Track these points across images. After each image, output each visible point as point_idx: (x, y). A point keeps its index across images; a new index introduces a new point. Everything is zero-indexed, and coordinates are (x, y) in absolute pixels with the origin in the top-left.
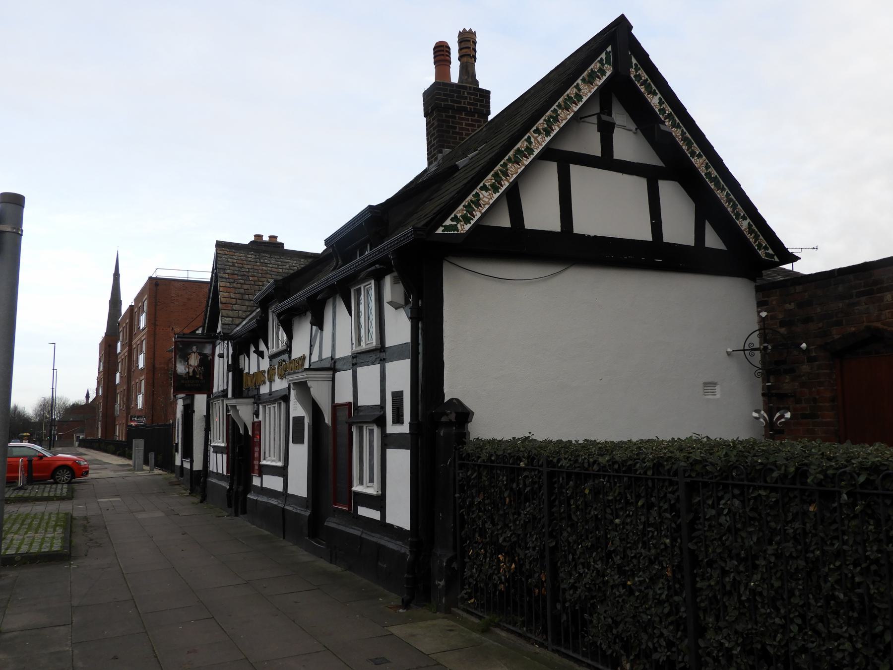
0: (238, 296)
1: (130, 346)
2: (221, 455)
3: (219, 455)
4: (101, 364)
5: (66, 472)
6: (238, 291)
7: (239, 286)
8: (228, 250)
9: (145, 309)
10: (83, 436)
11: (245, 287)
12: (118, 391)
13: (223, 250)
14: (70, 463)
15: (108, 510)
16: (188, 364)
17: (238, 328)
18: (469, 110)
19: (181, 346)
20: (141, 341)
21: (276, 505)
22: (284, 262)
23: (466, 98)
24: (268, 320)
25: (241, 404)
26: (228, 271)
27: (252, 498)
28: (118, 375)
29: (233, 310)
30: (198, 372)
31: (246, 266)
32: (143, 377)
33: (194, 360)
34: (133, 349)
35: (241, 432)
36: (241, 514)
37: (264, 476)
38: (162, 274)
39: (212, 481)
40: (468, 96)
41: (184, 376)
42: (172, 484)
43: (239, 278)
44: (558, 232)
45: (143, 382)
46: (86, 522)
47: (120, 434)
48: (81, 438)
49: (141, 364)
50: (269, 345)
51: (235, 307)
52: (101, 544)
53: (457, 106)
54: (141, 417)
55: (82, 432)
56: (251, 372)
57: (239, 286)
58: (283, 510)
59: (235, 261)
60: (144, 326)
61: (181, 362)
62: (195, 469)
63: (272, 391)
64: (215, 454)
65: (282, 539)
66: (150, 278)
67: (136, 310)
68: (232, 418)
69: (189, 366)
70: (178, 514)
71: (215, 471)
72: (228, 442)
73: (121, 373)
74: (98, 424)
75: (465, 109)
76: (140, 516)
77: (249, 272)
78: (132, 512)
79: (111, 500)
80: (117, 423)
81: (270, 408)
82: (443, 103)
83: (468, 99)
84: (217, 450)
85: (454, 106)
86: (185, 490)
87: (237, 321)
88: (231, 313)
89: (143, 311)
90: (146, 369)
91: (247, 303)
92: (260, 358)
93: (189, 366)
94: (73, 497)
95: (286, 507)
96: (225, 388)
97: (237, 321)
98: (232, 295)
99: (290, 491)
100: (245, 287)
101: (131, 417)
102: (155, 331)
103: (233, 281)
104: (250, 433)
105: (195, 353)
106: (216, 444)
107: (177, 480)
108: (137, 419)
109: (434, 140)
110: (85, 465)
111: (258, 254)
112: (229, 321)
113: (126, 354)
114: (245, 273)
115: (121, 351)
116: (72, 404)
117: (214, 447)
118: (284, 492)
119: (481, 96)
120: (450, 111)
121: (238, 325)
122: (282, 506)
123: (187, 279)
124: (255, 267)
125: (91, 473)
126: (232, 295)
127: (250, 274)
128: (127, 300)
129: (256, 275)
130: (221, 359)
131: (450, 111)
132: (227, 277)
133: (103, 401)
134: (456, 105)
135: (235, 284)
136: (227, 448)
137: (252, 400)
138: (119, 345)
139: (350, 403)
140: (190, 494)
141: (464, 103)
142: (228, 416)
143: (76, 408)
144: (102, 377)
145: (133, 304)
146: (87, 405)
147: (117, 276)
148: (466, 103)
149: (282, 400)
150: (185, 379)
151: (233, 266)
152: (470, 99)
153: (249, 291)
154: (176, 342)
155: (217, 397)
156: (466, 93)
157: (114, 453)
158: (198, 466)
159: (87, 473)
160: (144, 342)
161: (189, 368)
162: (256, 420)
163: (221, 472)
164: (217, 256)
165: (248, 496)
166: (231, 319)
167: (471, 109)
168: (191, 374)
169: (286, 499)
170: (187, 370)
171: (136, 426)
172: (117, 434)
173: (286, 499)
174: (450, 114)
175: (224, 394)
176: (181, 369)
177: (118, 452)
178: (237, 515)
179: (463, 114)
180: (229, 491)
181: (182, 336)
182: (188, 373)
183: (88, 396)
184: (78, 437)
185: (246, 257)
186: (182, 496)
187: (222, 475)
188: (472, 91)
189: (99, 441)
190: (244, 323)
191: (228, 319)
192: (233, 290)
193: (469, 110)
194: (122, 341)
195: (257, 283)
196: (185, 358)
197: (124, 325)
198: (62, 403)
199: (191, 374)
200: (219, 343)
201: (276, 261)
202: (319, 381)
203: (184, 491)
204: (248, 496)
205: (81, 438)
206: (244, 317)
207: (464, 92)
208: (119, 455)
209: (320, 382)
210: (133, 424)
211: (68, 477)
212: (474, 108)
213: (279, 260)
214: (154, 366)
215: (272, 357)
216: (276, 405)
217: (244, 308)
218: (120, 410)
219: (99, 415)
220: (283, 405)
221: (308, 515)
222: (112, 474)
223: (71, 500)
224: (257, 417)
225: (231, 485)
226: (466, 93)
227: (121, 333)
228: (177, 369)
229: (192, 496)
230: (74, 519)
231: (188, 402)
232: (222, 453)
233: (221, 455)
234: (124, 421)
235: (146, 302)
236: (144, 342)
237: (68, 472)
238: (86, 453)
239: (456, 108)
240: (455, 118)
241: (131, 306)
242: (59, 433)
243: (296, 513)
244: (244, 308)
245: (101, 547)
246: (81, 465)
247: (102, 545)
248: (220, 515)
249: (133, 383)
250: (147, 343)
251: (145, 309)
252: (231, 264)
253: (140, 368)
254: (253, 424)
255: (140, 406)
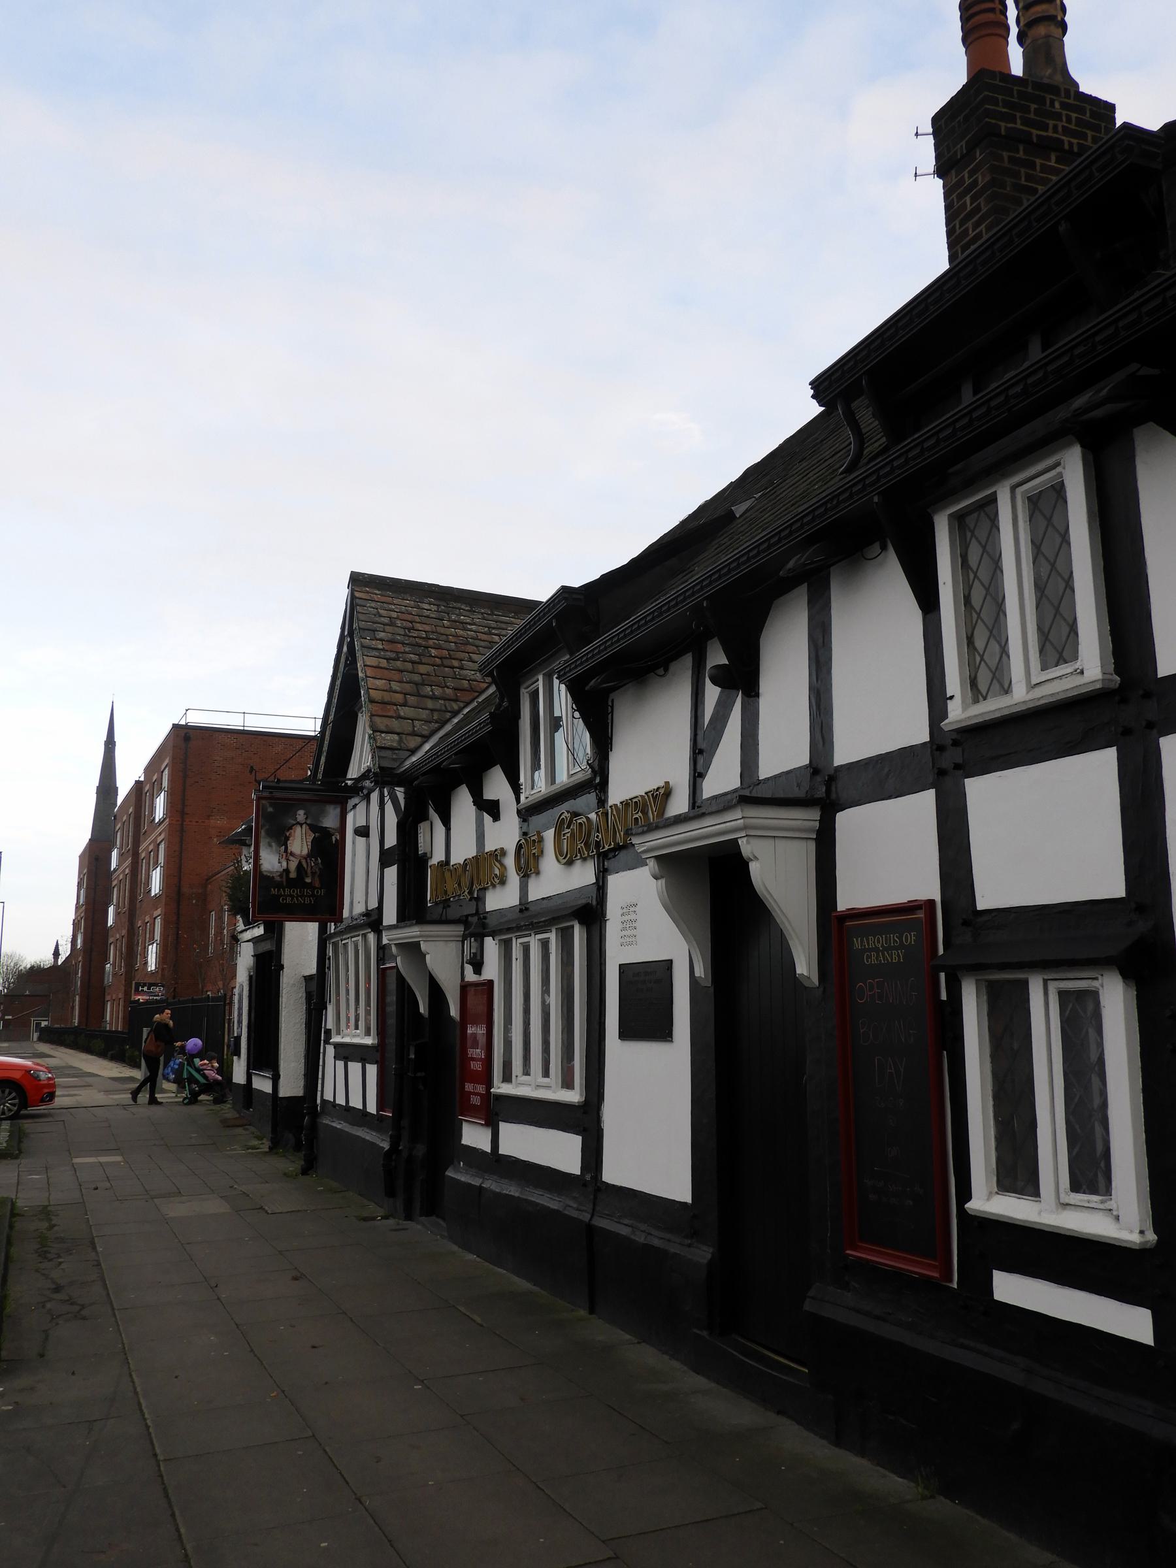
0: (408, 687)
1: (136, 854)
2: (360, 1065)
3: (355, 1067)
4: (82, 892)
5: (10, 1094)
6: (406, 677)
7: (409, 666)
8: (377, 592)
9: (165, 783)
10: (46, 1023)
11: (423, 669)
12: (111, 940)
13: (368, 592)
14: (17, 1075)
15: (96, 1189)
16: (286, 850)
17: (414, 759)
18: (1066, 147)
19: (270, 809)
20: (158, 846)
21: (558, 1211)
22: (502, 622)
23: (1058, 116)
24: (517, 716)
25: (429, 938)
26: (382, 635)
27: (463, 1179)
28: (111, 910)
29: (399, 717)
30: (309, 871)
31: (418, 626)
32: (159, 911)
33: (300, 842)
34: (140, 861)
35: (422, 1010)
36: (421, 1216)
37: (504, 1127)
38: (197, 719)
39: (334, 1125)
40: (1064, 112)
41: (278, 879)
42: (227, 1124)
43: (407, 649)
44: (319, 924)
45: (158, 921)
46: (46, 1225)
47: (113, 1017)
48: (43, 1026)
49: (156, 887)
50: (522, 780)
51: (403, 711)
52: (83, 1307)
53: (1037, 136)
54: (156, 985)
55: (45, 1015)
56: (457, 858)
57: (409, 666)
58: (590, 1229)
59: (394, 615)
60: (161, 815)
61: (270, 845)
62: (283, 1093)
63: (531, 898)
64: (340, 1064)
65: (582, 1313)
66: (175, 726)
67: (147, 788)
68: (401, 980)
69: (288, 854)
70: (261, 1208)
71: (341, 1100)
72: (381, 1033)
73: (117, 907)
74: (74, 1001)
75: (1056, 145)
76: (177, 1209)
77: (428, 638)
78: (152, 1198)
79: (103, 1159)
80: (108, 998)
81: (526, 949)
82: (1003, 124)
83: (1064, 119)
84: (346, 1053)
85: (1031, 133)
86: (260, 1138)
87: (412, 742)
88: (395, 724)
89: (161, 789)
90: (164, 896)
91: (430, 704)
92: (487, 818)
93: (288, 854)
94: (20, 1152)
95: (602, 1223)
96: (373, 904)
97: (412, 742)
98: (395, 686)
99: (610, 1175)
100: (423, 669)
101: (138, 985)
102: (182, 824)
103: (393, 655)
104: (454, 1011)
105: (301, 825)
106: (347, 1040)
107: (238, 1116)
108: (149, 989)
109: (977, 225)
110: (49, 1079)
111: (445, 604)
112: (392, 741)
113: (127, 871)
114: (420, 641)
115: (119, 865)
116: (29, 966)
117: (337, 1046)
118: (588, 1177)
119: (1094, 114)
120: (1021, 148)
121: (413, 752)
122: (586, 1217)
123: (242, 728)
124: (440, 629)
125: (59, 1096)
126: (395, 686)
127: (431, 642)
128: (127, 778)
129: (444, 646)
130: (361, 841)
131: (1021, 148)
132: (380, 647)
133: (83, 957)
134: (1035, 132)
135: (398, 664)
136: (380, 1047)
137: (459, 929)
138: (115, 854)
139: (931, 903)
140: (270, 1148)
141: (1055, 127)
142: (382, 974)
143: (35, 973)
144: (82, 915)
145: (142, 779)
146: (54, 968)
147: (110, 744)
148: (1060, 129)
149: (576, 918)
150: (279, 885)
151: (392, 624)
152: (1069, 120)
153: (433, 678)
154: (259, 799)
155: (353, 928)
156: (1057, 105)
157: (102, 1054)
158: (291, 1085)
159: (52, 1096)
160: (162, 847)
161: (288, 860)
162: (470, 976)
163: (360, 1107)
164: (353, 605)
165: (450, 1173)
166: (396, 737)
167: (1071, 144)
168: (293, 875)
169: (595, 1198)
170: (284, 864)
171: (147, 1002)
172: (108, 1019)
173: (595, 1198)
174: (1021, 154)
175: (373, 920)
176: (271, 861)
177: (110, 1053)
178: (409, 1217)
179: (1053, 158)
180: (388, 1154)
181: (274, 784)
182: (287, 871)
183: (56, 954)
184: (38, 1025)
185: (418, 607)
186: (252, 1153)
187: (364, 1113)
188: (1071, 101)
189: (75, 1031)
190: (427, 747)
191: (389, 736)
192: (396, 675)
193: (1066, 147)
194: (121, 848)
195: (447, 662)
196: (280, 837)
197: (125, 818)
198: (12, 964)
199: (293, 875)
200: (355, 806)
201: (484, 618)
202: (777, 841)
203: (255, 1143)
204: (450, 1173)
205: (43, 1026)
206: (425, 733)
207: (1052, 102)
208: (113, 1058)
209: (781, 844)
210: (141, 998)
211: (14, 1105)
212: (1078, 143)
213: (490, 617)
214: (179, 893)
215: (526, 814)
216: (552, 936)
217: (424, 714)
218: (115, 975)
219: (76, 983)
220: (578, 934)
221: (705, 1261)
222: (99, 1098)
223: (16, 1157)
224: (478, 969)
225: (395, 1143)
226: (1057, 105)
227: (119, 834)
228: (261, 862)
229: (276, 1153)
230: (18, 1215)
231: (267, 946)
232: (364, 1061)
233: (360, 1065)
234: (121, 995)
235: (166, 772)
236: (162, 847)
237: (14, 1094)
238: (52, 1053)
239: (1035, 140)
240: (1032, 165)
241: (137, 782)
242: (6, 1017)
243: (648, 1248)
244: (424, 714)
245: (84, 1318)
246: (40, 1080)
247: (84, 1313)
248: (365, 1214)
249: (139, 924)
250: (167, 849)
251: (165, 783)
252: (386, 620)
253: (153, 894)
254: (465, 987)
255: (152, 965)
